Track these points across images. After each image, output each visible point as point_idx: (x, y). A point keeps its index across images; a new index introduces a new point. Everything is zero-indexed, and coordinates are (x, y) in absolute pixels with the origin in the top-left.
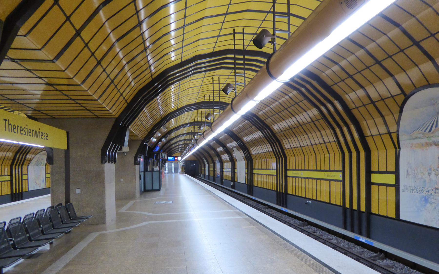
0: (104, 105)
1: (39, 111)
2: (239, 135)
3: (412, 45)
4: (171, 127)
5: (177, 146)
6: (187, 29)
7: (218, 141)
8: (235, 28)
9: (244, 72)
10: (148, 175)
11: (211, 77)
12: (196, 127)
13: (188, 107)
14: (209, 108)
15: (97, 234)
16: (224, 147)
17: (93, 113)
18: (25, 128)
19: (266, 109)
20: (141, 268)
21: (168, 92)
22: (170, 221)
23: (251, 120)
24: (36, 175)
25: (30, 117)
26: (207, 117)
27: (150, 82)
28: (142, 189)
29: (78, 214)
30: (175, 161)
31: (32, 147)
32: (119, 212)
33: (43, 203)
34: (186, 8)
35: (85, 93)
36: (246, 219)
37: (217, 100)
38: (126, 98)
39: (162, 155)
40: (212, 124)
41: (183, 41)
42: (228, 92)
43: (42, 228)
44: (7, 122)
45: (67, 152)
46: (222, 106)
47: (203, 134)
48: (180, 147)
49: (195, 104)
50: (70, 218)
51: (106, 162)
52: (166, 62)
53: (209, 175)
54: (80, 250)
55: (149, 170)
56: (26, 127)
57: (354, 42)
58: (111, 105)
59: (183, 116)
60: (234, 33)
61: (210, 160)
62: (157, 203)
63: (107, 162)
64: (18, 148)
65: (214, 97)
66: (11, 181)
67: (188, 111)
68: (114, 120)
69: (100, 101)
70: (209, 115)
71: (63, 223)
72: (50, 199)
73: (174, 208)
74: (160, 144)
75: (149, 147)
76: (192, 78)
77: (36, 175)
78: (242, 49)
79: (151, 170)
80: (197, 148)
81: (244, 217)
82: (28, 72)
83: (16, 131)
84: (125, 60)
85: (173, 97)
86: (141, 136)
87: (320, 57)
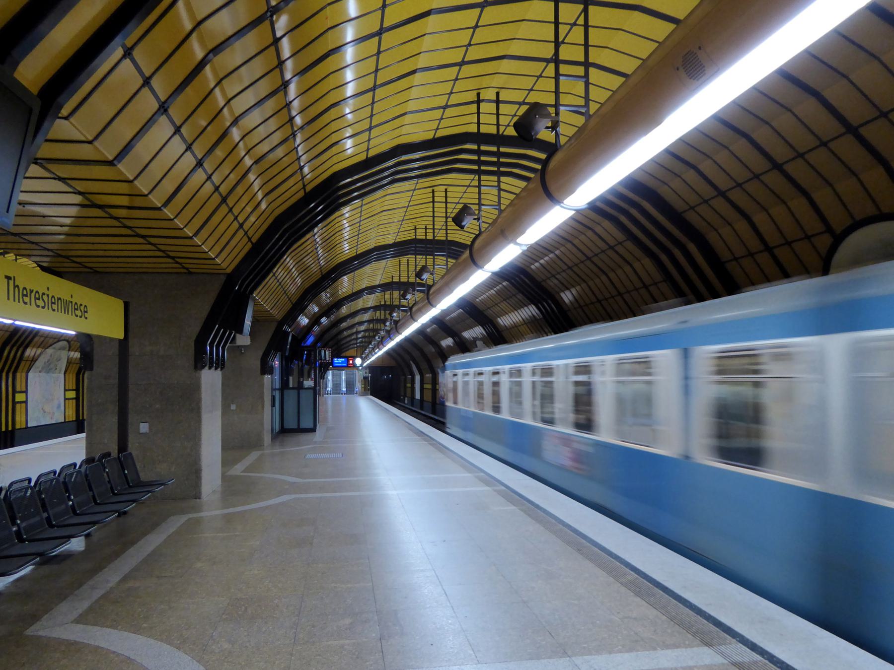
0: (179, 223)
1: (67, 257)
2: (489, 313)
3: (862, 125)
4: (340, 292)
5: (353, 334)
6: (380, 93)
7: (442, 324)
8: (481, 91)
9: (499, 179)
10: (291, 396)
11: (430, 190)
12: (396, 293)
13: (379, 252)
14: (426, 253)
15: (184, 519)
16: (457, 339)
17: (180, 264)
18: (43, 294)
19: (546, 258)
20: (280, 585)
21: (336, 221)
22: (338, 494)
23: (515, 280)
24: (44, 394)
25: (43, 269)
26: (419, 275)
27: (301, 199)
28: (277, 427)
29: (144, 476)
30: (347, 366)
31: (39, 331)
32: (229, 473)
33: (70, 451)
34: (379, 52)
35: (197, 249)
36: (499, 492)
37: (441, 236)
38: (250, 233)
39: (320, 354)
40: (430, 287)
41: (372, 116)
42: (463, 224)
43: (18, 525)
44: (11, 282)
45: (123, 344)
46: (452, 249)
47: (411, 309)
48: (360, 336)
49: (395, 245)
50: (128, 484)
51: (203, 367)
52: (335, 159)
53: (422, 399)
54: (150, 549)
55: (291, 386)
56: (46, 292)
57: (731, 126)
58: (217, 249)
59: (367, 269)
60: (478, 101)
61: (424, 366)
62: (308, 456)
63: (207, 368)
64: (8, 334)
65: (436, 231)
66: (77, 399)
67: (378, 259)
68: (223, 278)
69: (168, 212)
70: (424, 269)
71: (114, 494)
72: (83, 444)
73: (348, 468)
74: (316, 329)
75: (293, 336)
76: (390, 191)
77: (44, 394)
78: (495, 132)
79: (296, 386)
80: (398, 339)
81: (495, 488)
82: (60, 183)
83: (27, 299)
84: (251, 158)
85: (348, 229)
86: (278, 314)
87: (827, 36)
